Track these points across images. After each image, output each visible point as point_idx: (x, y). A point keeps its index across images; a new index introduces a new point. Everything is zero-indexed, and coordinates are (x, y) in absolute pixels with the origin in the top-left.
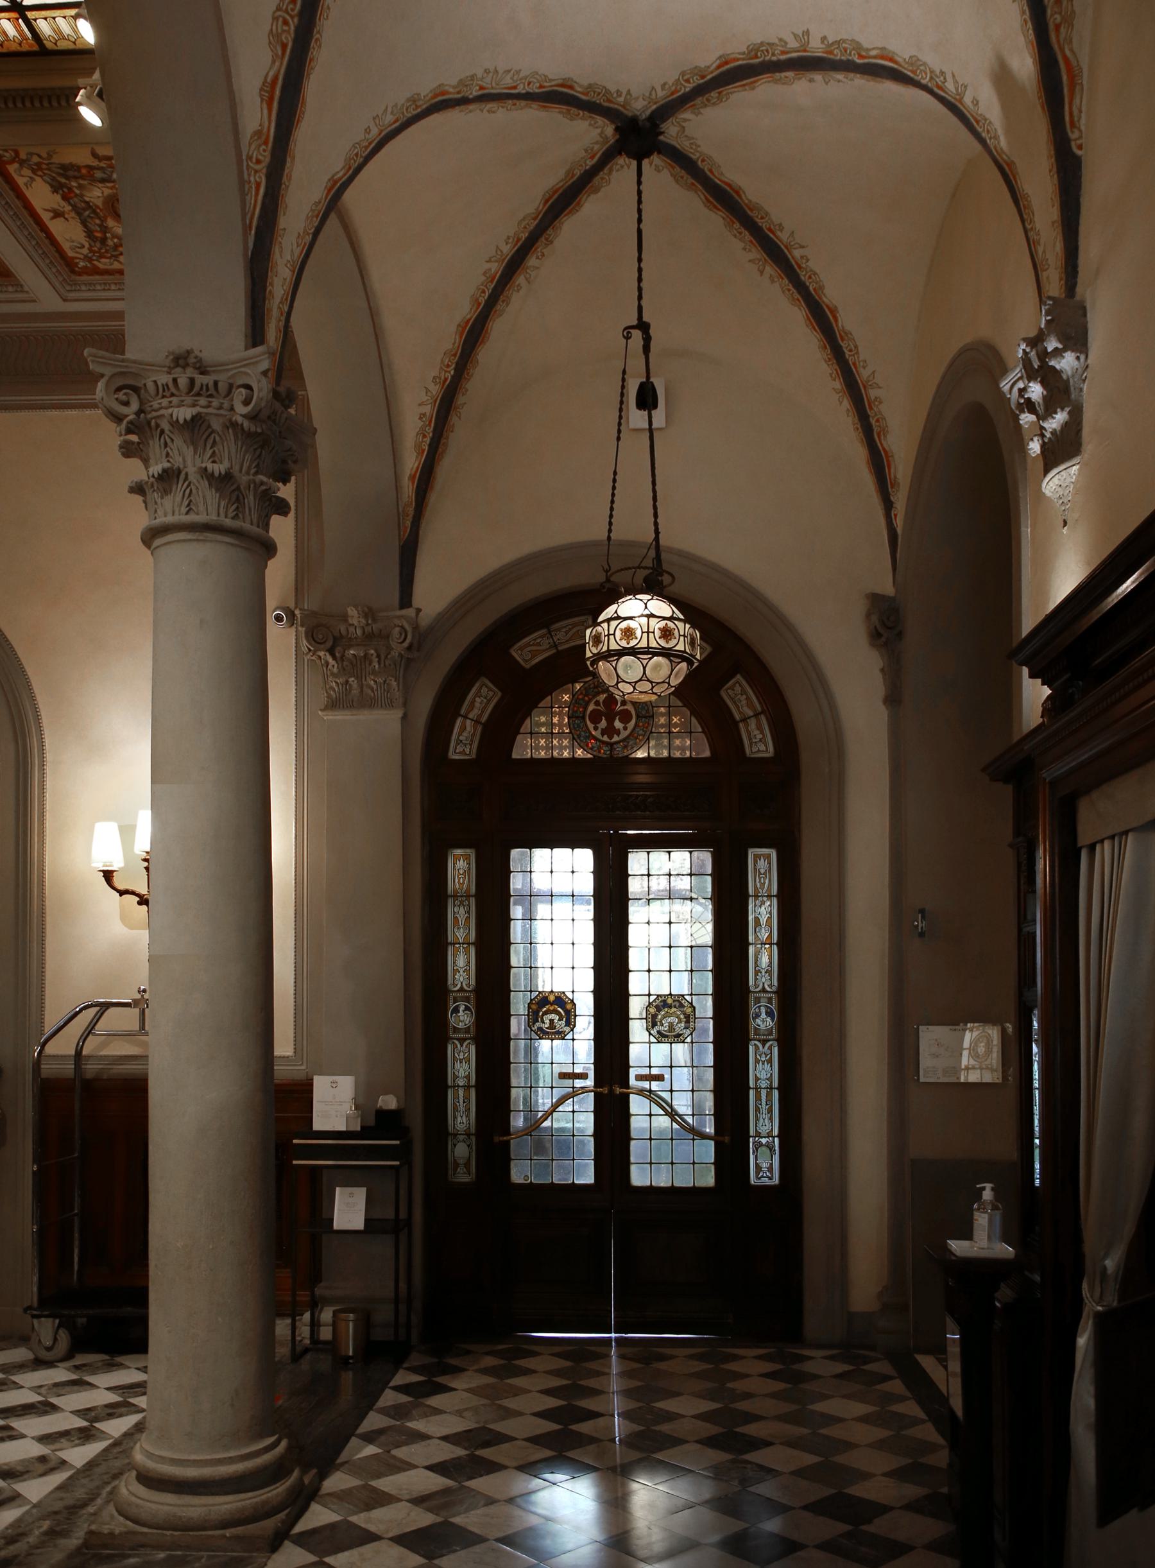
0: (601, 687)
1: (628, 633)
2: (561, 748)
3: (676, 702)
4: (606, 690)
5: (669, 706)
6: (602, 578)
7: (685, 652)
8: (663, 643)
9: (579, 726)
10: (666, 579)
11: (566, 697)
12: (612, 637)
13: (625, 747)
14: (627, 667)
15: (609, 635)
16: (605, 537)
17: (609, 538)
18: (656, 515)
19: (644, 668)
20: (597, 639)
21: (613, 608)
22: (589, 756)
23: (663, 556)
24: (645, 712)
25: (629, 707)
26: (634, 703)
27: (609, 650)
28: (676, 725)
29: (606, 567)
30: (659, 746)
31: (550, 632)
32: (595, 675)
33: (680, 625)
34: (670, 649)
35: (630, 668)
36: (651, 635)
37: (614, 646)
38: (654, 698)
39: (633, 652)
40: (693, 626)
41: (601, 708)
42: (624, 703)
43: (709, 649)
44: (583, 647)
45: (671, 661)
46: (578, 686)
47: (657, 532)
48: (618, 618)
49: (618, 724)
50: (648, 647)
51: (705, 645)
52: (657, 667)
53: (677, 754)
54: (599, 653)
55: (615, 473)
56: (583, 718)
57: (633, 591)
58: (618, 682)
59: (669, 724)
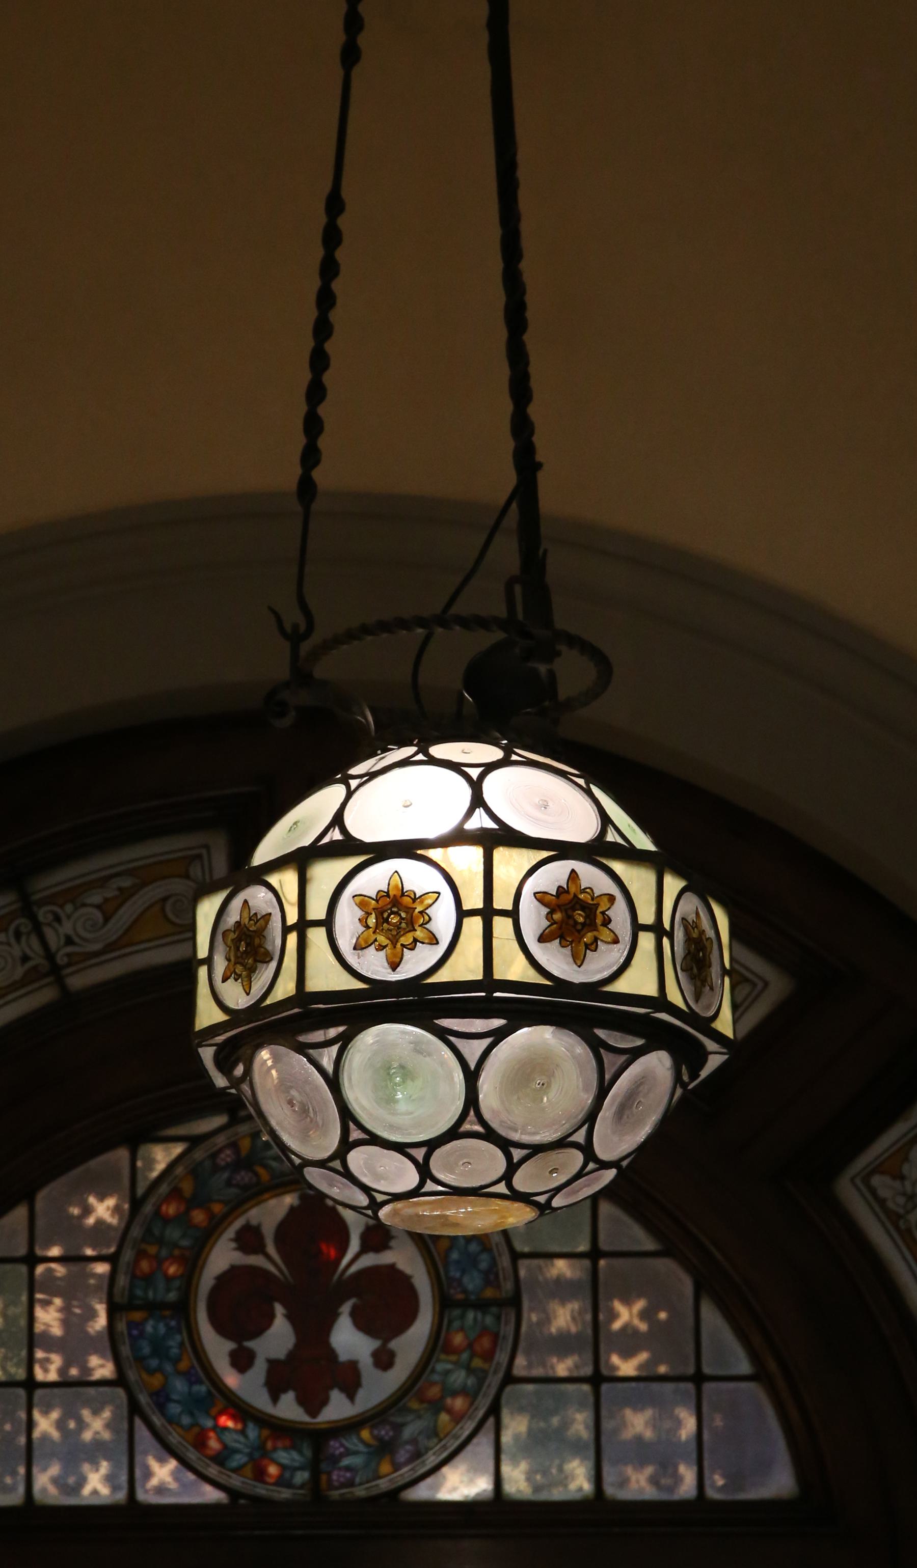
0: (264, 1164)
1: (396, 916)
2: (76, 1454)
3: (625, 1231)
4: (290, 1174)
5: (595, 1254)
6: (272, 664)
7: (660, 1002)
8: (557, 961)
9: (159, 1350)
10: (571, 673)
11: (103, 1210)
12: (317, 936)
13: (384, 1448)
14: (390, 1072)
15: (303, 925)
16: (288, 476)
17: (307, 488)
18: (521, 390)
19: (472, 1077)
20: (248, 946)
21: (321, 804)
22: (211, 1495)
23: (559, 564)
24: (480, 1286)
25: (403, 1258)
26: (425, 1243)
27: (302, 996)
28: (629, 1342)
29: (293, 617)
30: (545, 1443)
31: (27, 909)
32: (240, 1108)
33: (639, 880)
34: (593, 990)
35: (403, 1080)
36: (503, 926)
37: (326, 976)
38: (518, 1216)
39: (421, 1003)
40: (699, 885)
41: (271, 1261)
42: (378, 1237)
43: (777, 986)
44: (187, 968)
45: (596, 1046)
46: (161, 1157)
47: (526, 462)
48: (350, 846)
49: (348, 1339)
50: (489, 982)
51: (756, 964)
52: (531, 1074)
53: (637, 1484)
54: (255, 1010)
55: (335, 204)
56: (182, 1310)
57: (418, 726)
58: (346, 1145)
59: (596, 1338)
